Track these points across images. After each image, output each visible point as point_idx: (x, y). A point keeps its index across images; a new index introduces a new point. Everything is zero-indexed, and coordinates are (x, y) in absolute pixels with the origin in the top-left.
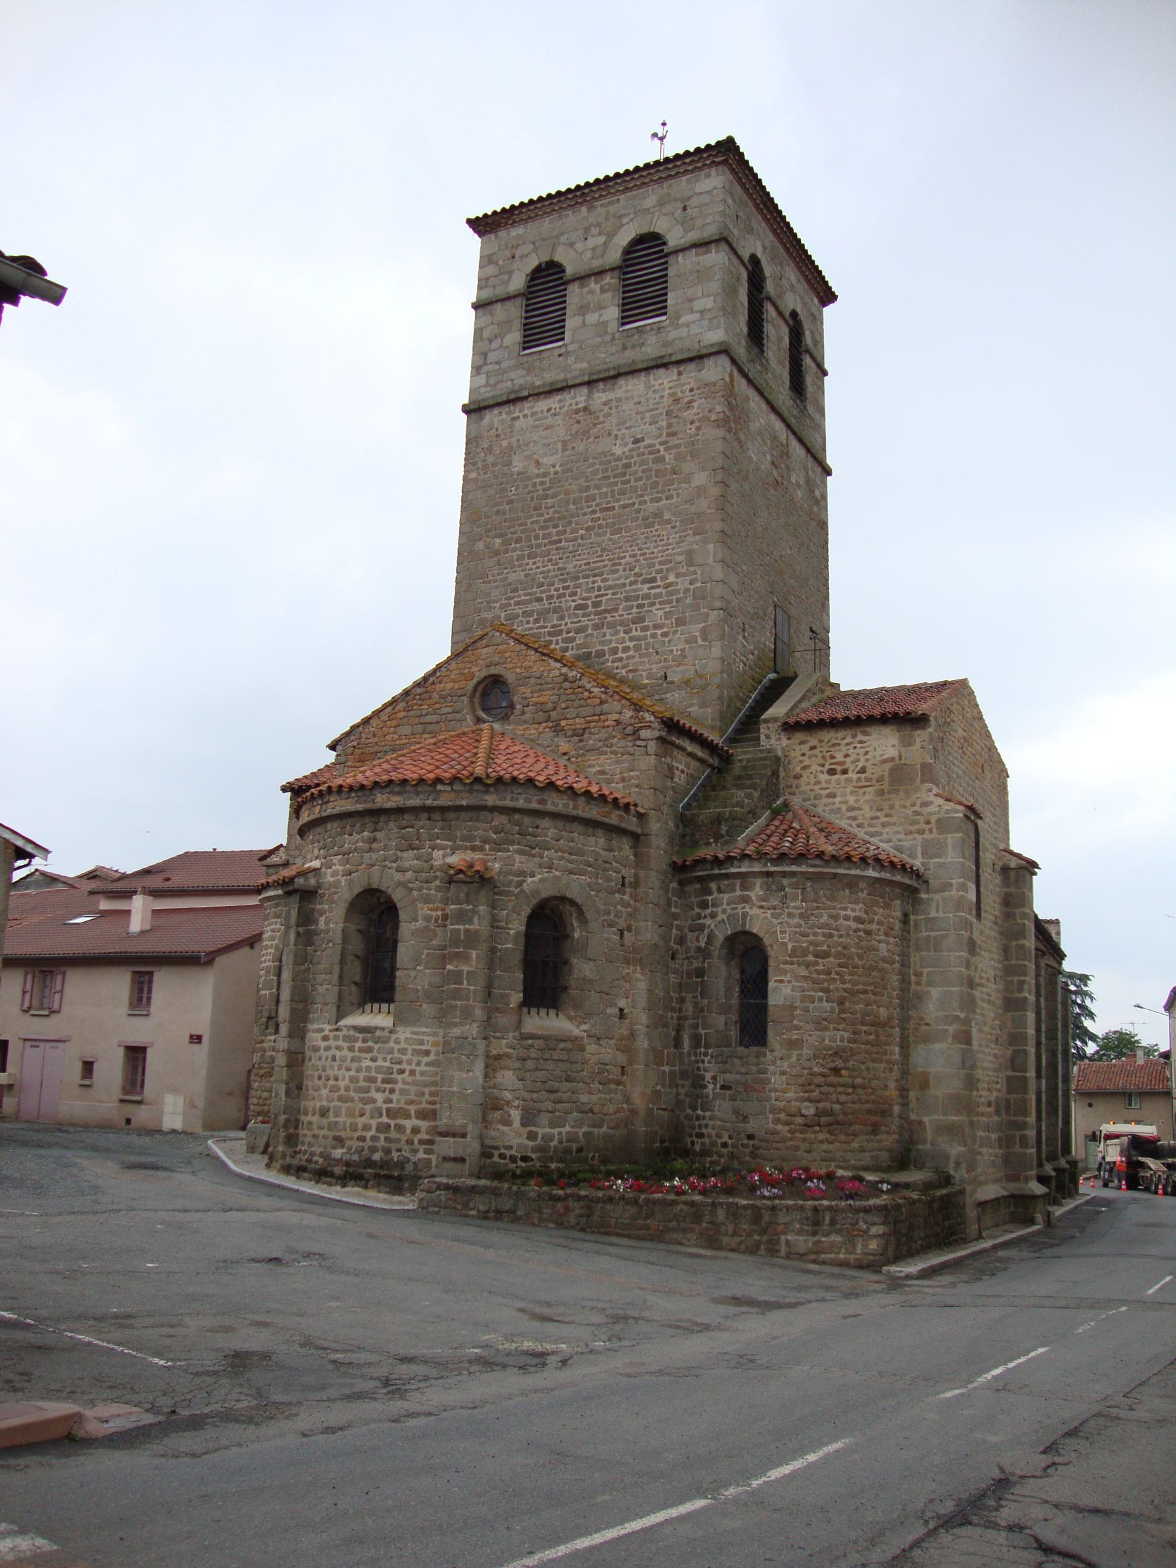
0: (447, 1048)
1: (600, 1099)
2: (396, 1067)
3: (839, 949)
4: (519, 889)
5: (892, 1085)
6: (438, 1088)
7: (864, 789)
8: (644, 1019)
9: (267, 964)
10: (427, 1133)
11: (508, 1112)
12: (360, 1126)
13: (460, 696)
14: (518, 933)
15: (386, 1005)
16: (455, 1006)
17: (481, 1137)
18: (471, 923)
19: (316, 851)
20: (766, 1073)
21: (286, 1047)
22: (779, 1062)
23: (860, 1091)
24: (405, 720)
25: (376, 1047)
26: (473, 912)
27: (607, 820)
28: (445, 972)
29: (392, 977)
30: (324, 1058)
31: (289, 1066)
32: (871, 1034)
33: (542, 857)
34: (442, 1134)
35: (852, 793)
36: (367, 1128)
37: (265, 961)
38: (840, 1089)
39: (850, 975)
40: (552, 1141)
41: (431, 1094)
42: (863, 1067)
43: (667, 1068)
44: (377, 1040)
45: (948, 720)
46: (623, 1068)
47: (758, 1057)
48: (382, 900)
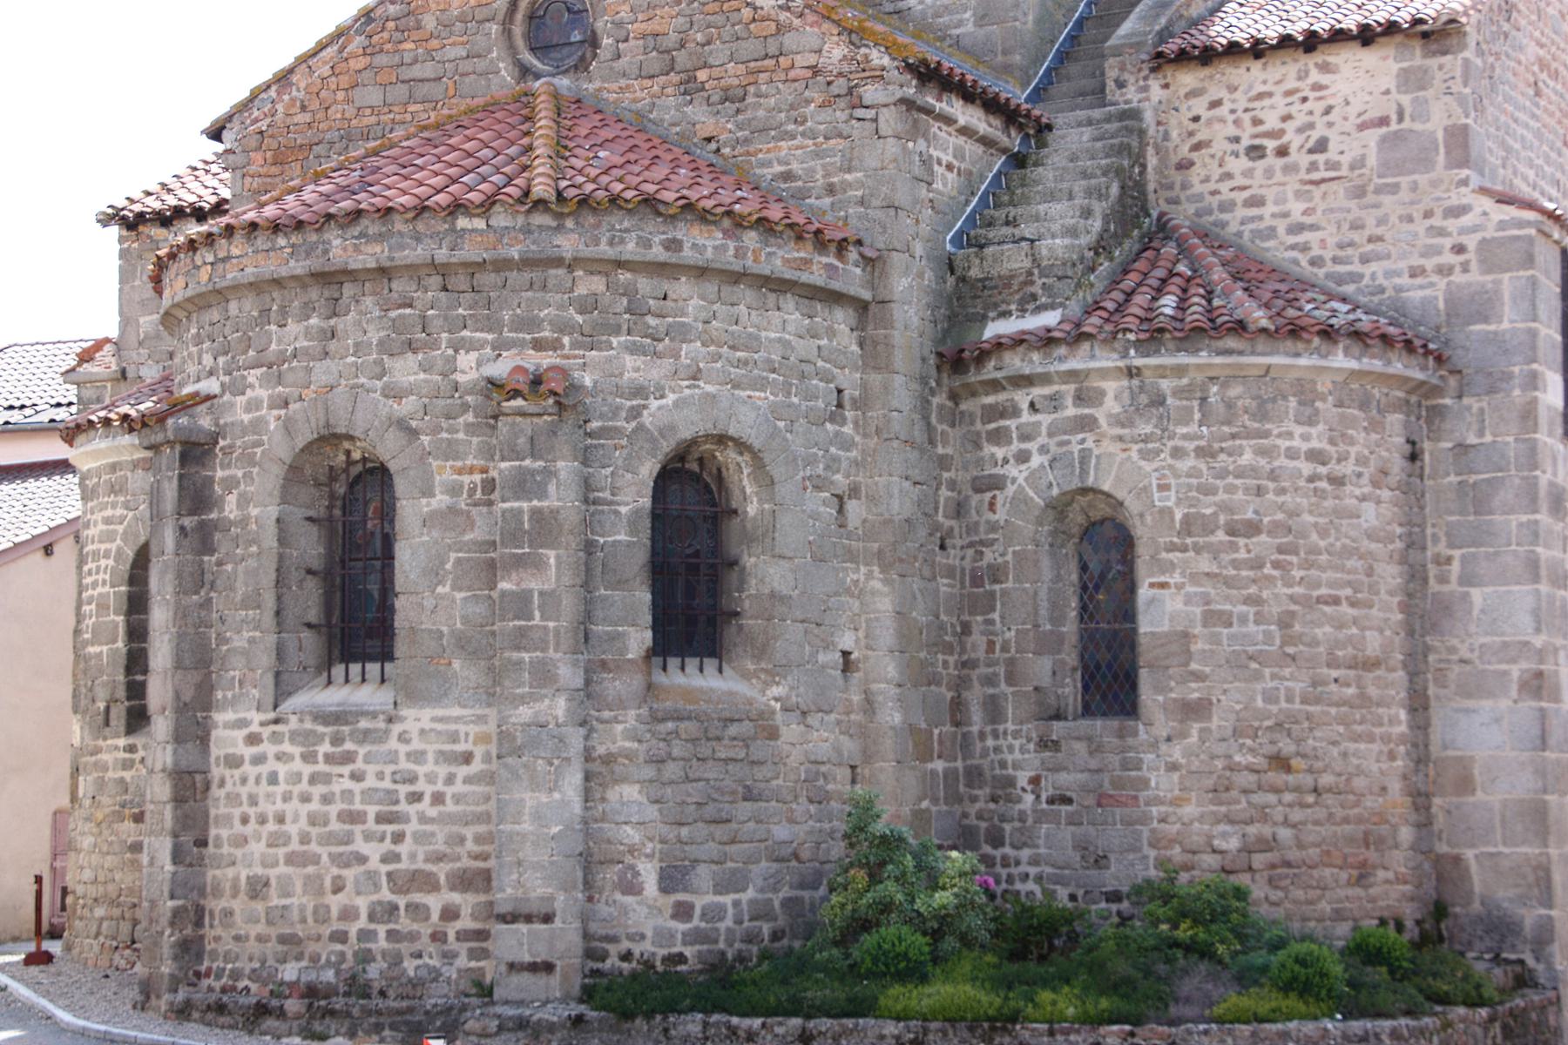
0: (508, 745)
1: (810, 833)
2: (403, 790)
3: (1280, 516)
4: (634, 424)
5: (1395, 786)
6: (492, 827)
7: (1323, 187)
8: (891, 670)
9: (100, 590)
10: (474, 917)
11: (632, 867)
12: (335, 912)
13: (480, 22)
14: (636, 512)
15: (377, 666)
16: (520, 662)
17: (585, 919)
18: (543, 495)
19: (208, 360)
20: (1139, 769)
21: (169, 760)
22: (1164, 747)
23: (1329, 799)
24: (367, 75)
25: (362, 751)
26: (549, 473)
27: (805, 277)
28: (495, 594)
29: (386, 610)
30: (252, 780)
31: (178, 800)
32: (1348, 685)
33: (677, 357)
34: (505, 918)
35: (1298, 195)
36: (348, 914)
37: (95, 585)
38: (1288, 797)
39: (1300, 567)
40: (721, 919)
41: (478, 839)
42: (1335, 751)
43: (939, 765)
44: (365, 737)
45: (1506, 27)
46: (853, 768)
47: (1121, 737)
48: (356, 455)
